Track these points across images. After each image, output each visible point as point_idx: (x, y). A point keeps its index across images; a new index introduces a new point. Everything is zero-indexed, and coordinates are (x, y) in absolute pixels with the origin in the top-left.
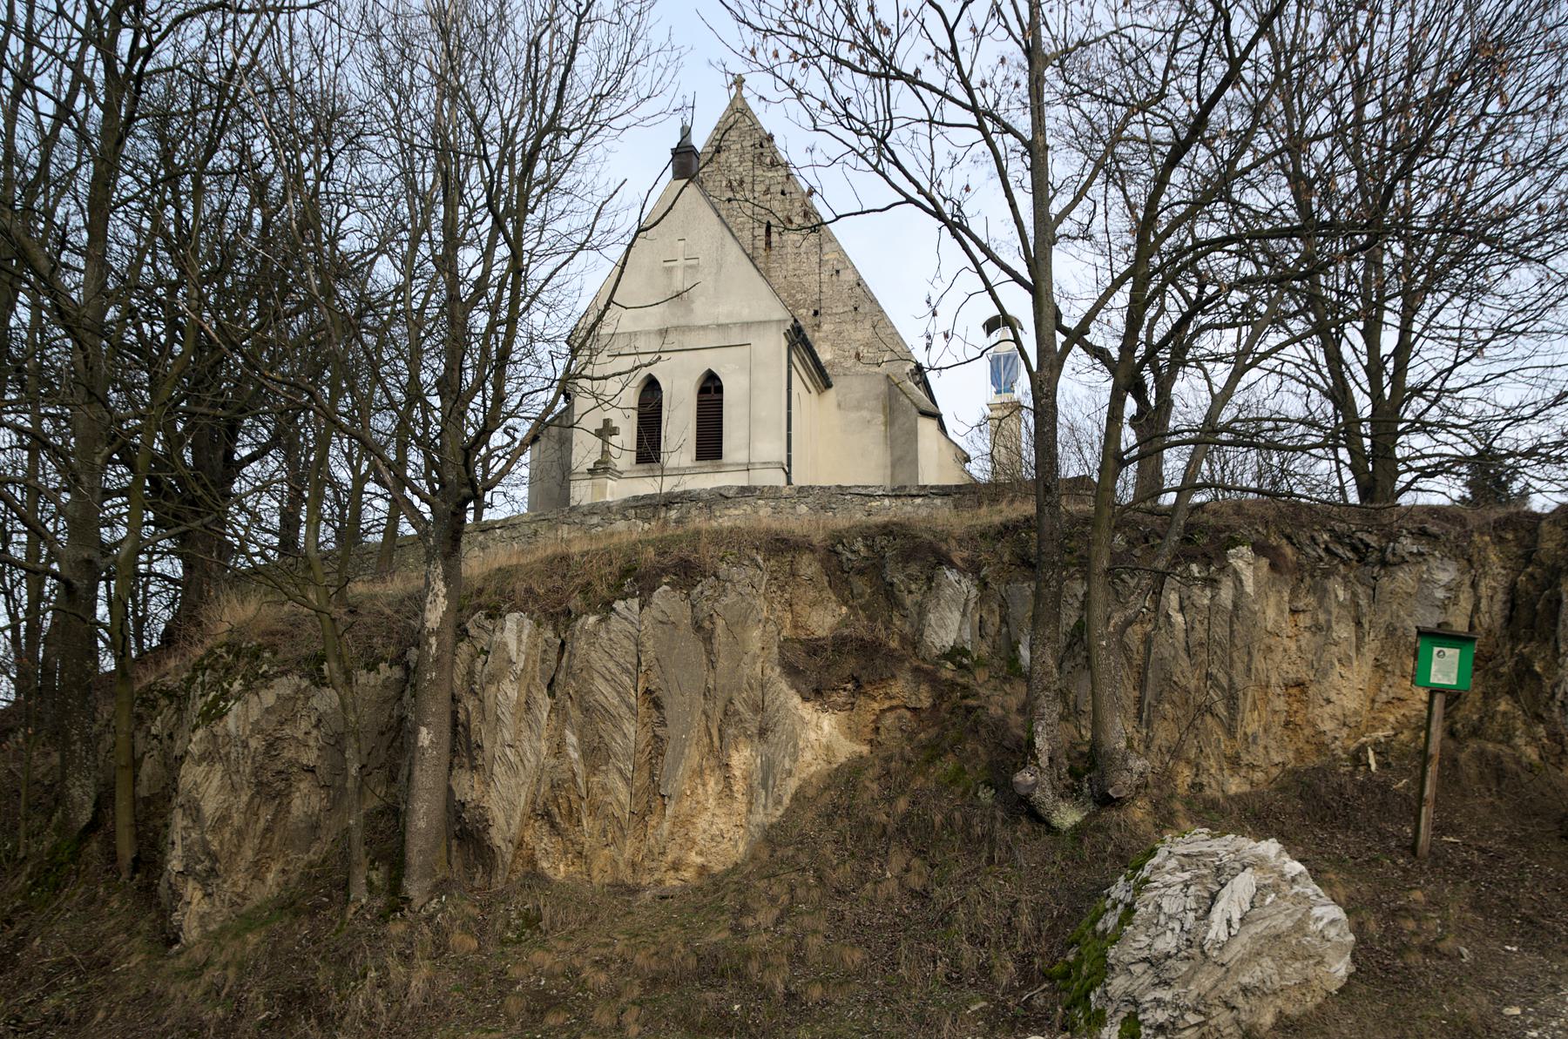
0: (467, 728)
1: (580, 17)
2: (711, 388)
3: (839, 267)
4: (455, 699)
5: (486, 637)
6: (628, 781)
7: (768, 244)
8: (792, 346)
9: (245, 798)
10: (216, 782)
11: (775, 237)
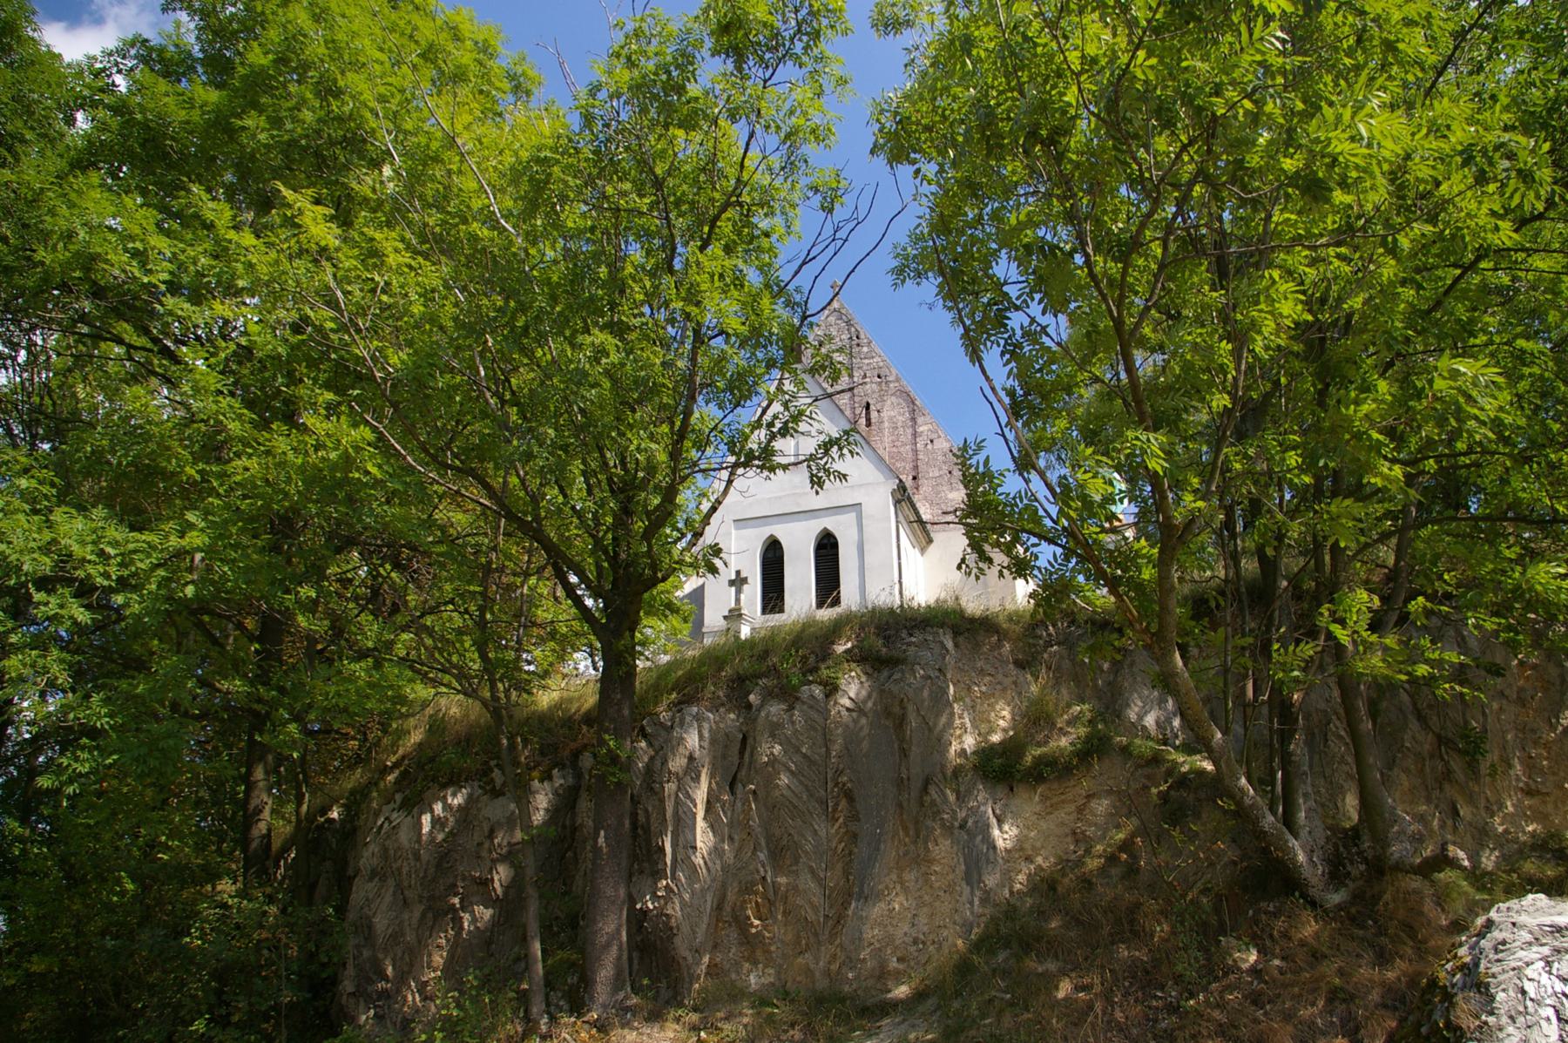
0: (647, 830)
1: (765, 81)
2: (827, 548)
3: (934, 436)
4: (635, 801)
5: (663, 733)
6: (821, 882)
7: (868, 420)
8: (897, 502)
9: (417, 914)
10: (388, 898)
11: (874, 415)
